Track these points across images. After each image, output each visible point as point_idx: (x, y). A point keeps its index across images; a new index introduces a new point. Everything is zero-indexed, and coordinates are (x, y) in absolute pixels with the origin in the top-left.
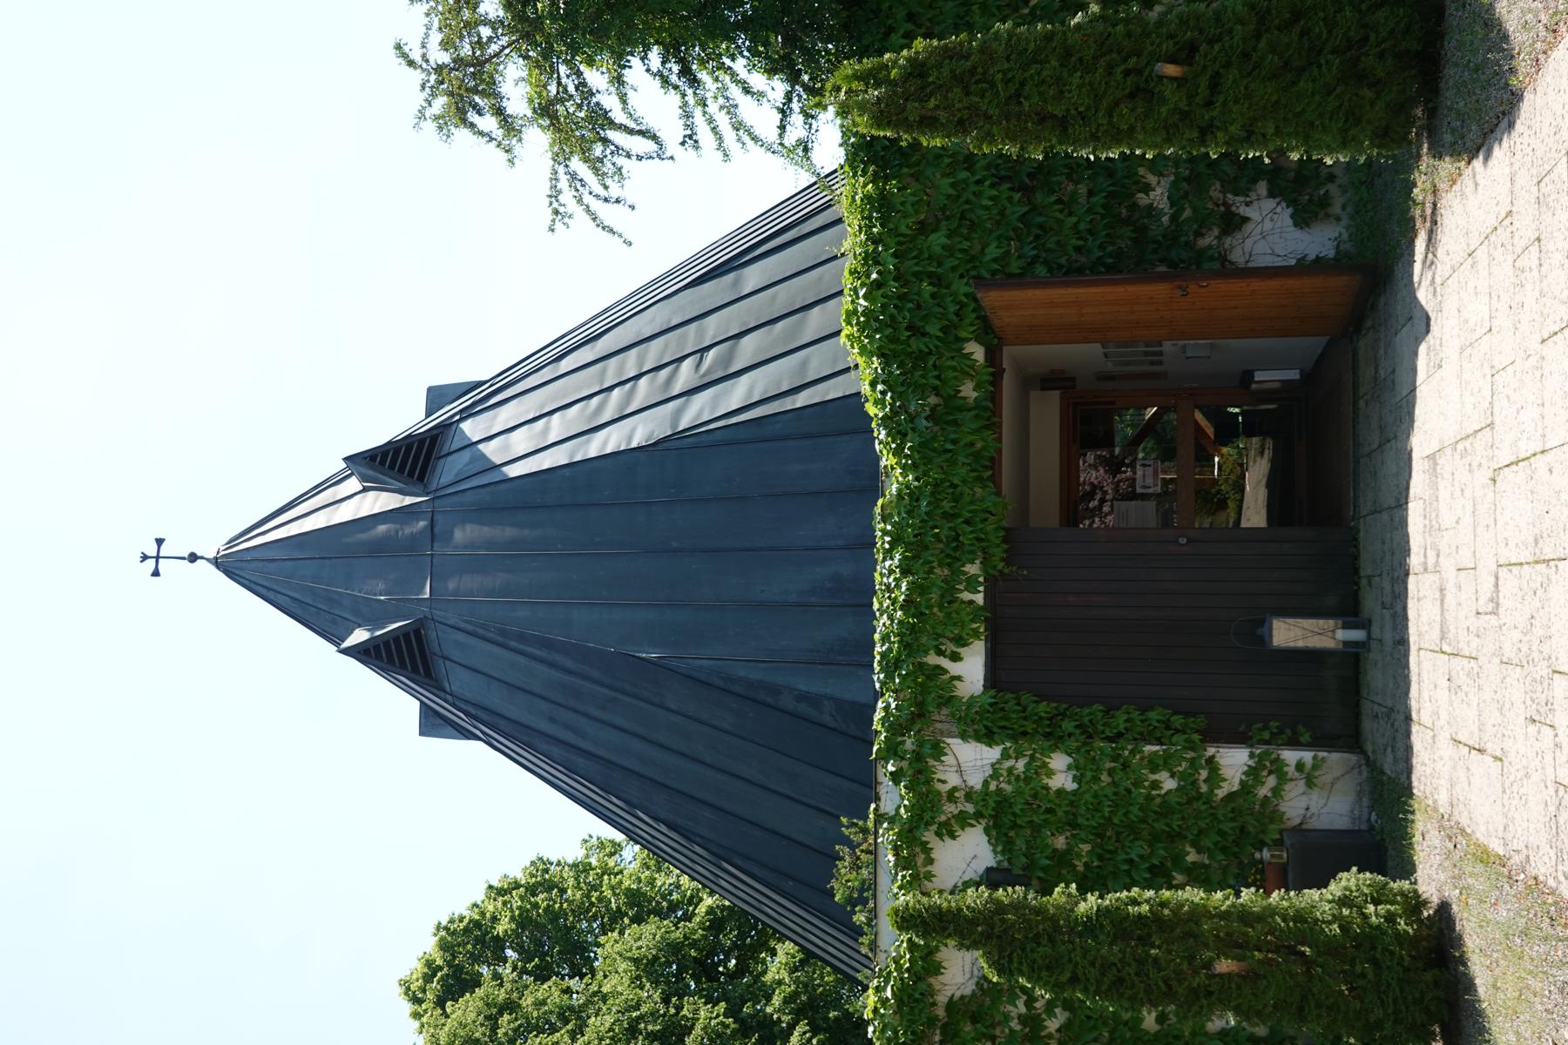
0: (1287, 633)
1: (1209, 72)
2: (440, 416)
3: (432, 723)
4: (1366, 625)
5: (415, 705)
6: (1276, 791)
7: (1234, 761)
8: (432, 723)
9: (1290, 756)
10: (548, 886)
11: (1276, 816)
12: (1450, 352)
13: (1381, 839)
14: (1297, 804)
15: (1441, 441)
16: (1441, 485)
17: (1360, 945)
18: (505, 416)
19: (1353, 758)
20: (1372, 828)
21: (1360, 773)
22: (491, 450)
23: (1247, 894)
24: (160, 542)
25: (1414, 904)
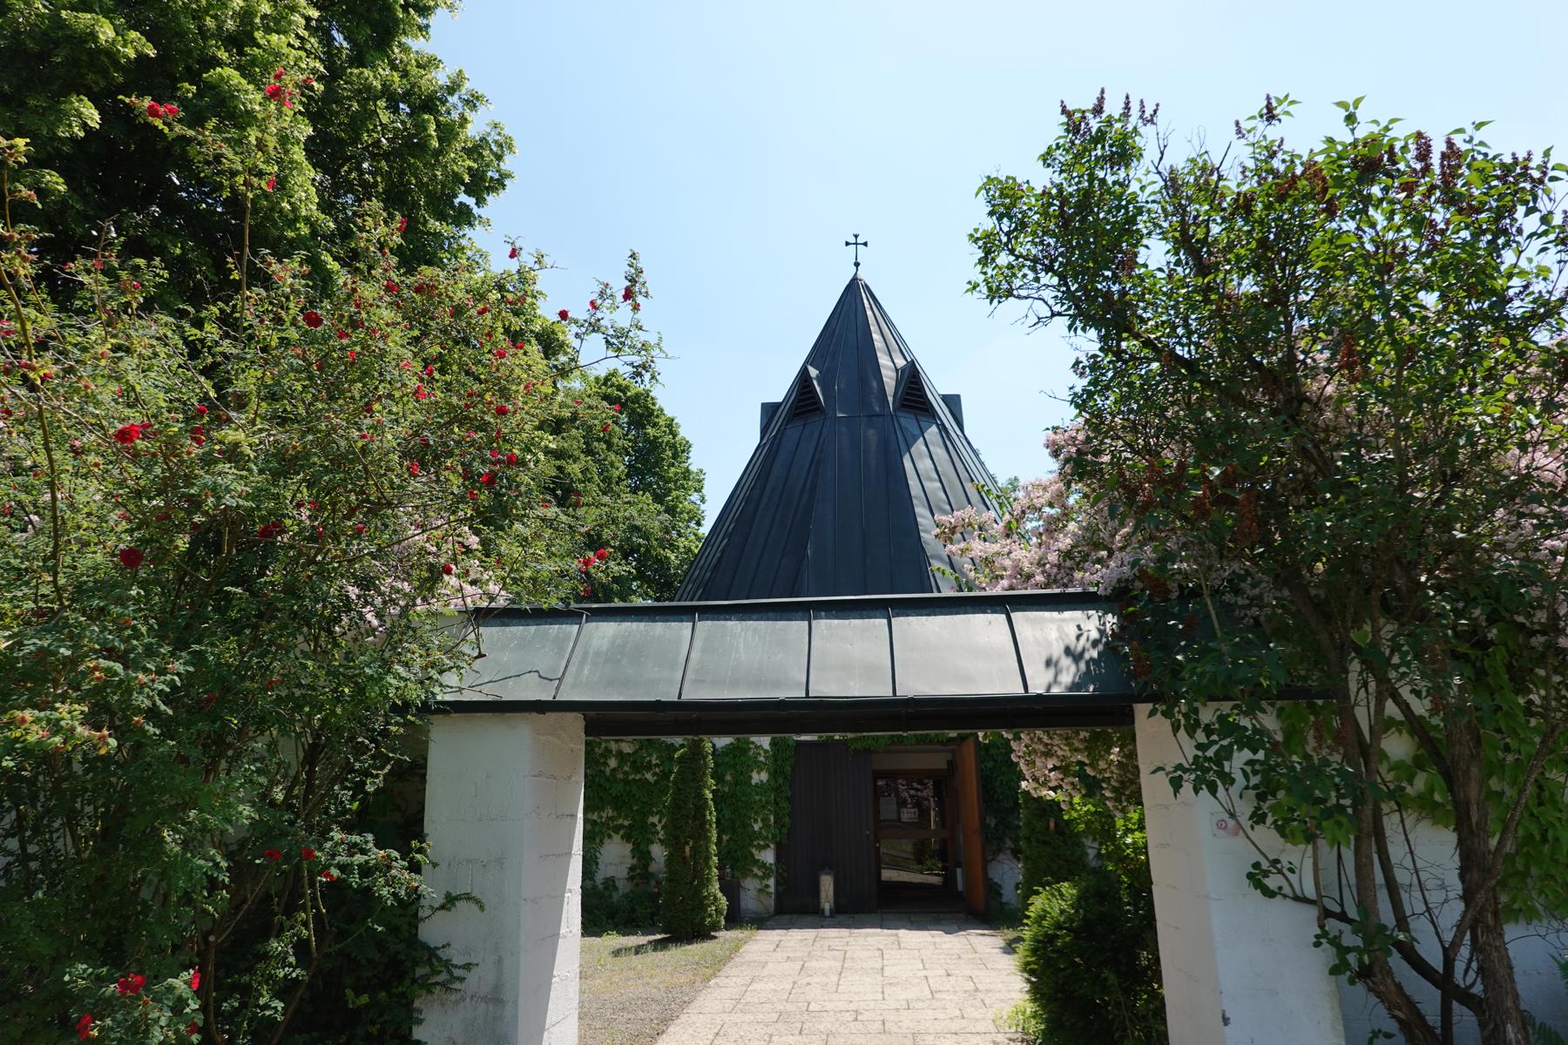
0: (827, 884)
3: (769, 410)
5: (779, 397)
6: (756, 876)
7: (768, 856)
8: (769, 410)
9: (771, 882)
10: (675, 456)
11: (745, 876)
12: (937, 940)
13: (736, 919)
14: (750, 885)
17: (699, 903)
18: (939, 452)
22: (919, 446)
23: (715, 859)
24: (865, 244)
25: (715, 927)
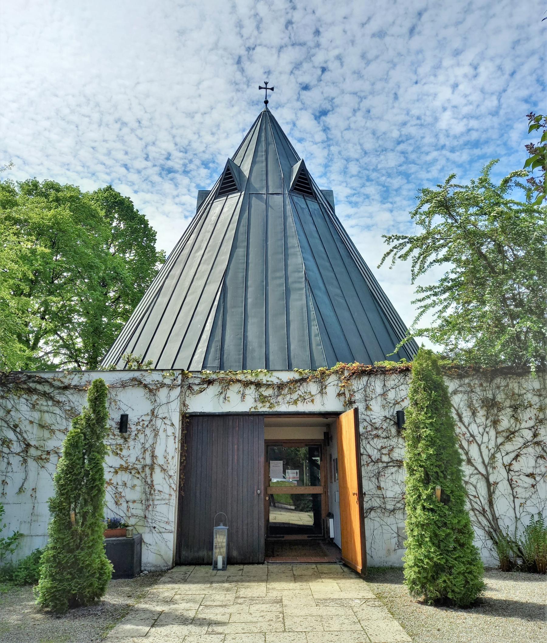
1: (436, 509)
2: (320, 196)
4: (224, 569)
15: (286, 606)
16: (268, 606)
19: (170, 563)
20: (142, 572)
21: (164, 566)
